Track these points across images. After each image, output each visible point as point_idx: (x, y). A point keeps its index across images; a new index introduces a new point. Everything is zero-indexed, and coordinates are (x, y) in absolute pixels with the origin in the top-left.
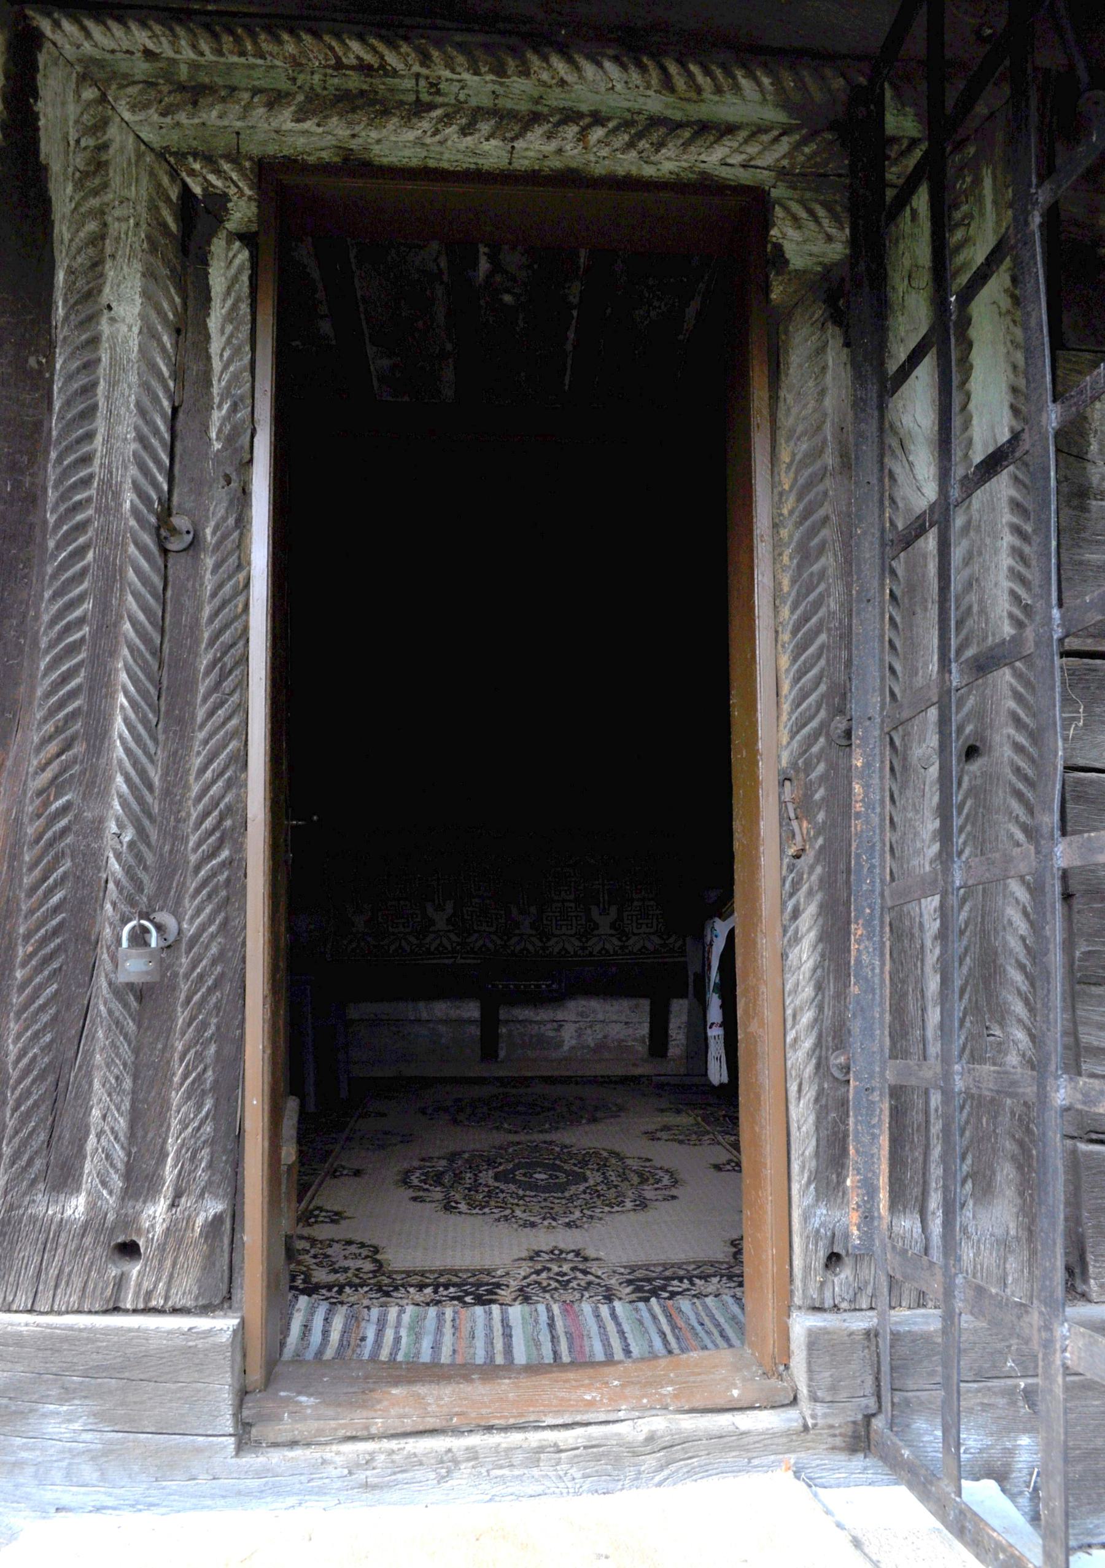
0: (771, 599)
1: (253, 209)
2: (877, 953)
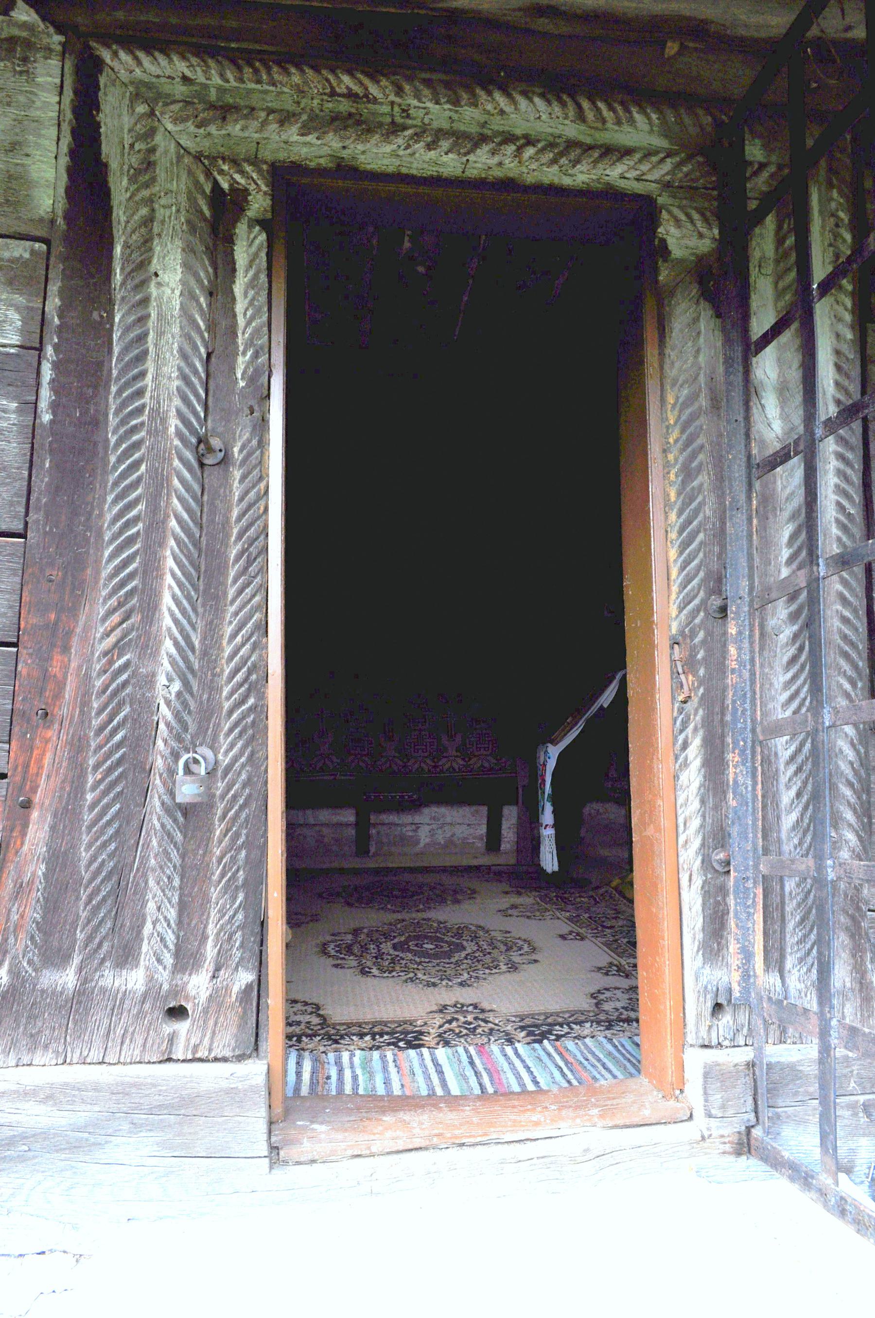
1: (267, 202)
2: (749, 775)
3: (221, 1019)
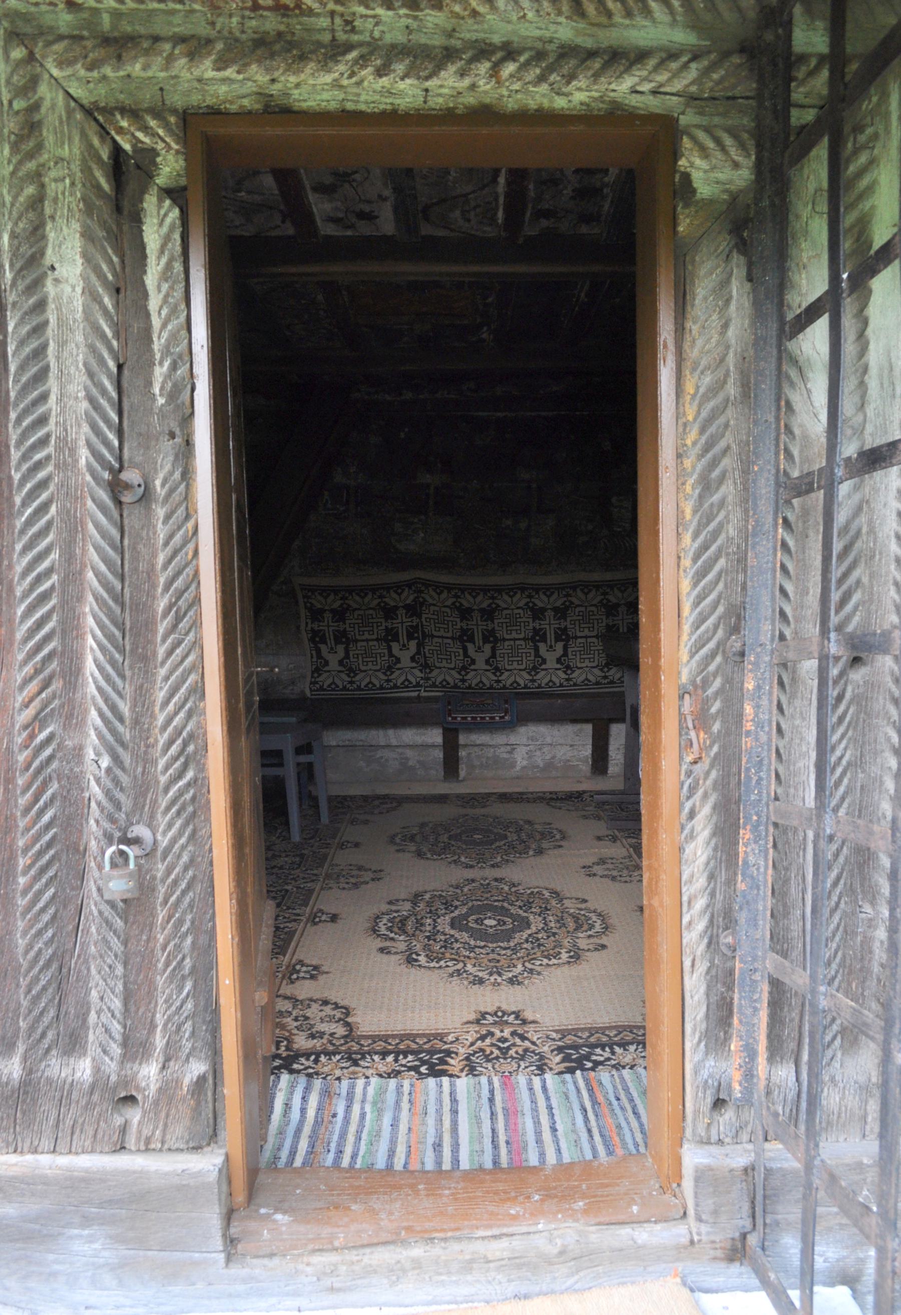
0: (674, 527)
3: (173, 1111)
